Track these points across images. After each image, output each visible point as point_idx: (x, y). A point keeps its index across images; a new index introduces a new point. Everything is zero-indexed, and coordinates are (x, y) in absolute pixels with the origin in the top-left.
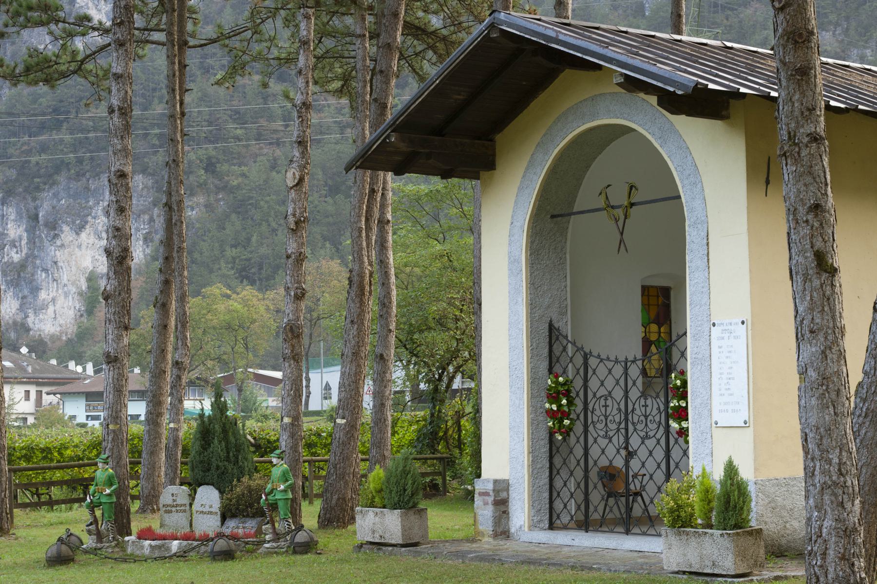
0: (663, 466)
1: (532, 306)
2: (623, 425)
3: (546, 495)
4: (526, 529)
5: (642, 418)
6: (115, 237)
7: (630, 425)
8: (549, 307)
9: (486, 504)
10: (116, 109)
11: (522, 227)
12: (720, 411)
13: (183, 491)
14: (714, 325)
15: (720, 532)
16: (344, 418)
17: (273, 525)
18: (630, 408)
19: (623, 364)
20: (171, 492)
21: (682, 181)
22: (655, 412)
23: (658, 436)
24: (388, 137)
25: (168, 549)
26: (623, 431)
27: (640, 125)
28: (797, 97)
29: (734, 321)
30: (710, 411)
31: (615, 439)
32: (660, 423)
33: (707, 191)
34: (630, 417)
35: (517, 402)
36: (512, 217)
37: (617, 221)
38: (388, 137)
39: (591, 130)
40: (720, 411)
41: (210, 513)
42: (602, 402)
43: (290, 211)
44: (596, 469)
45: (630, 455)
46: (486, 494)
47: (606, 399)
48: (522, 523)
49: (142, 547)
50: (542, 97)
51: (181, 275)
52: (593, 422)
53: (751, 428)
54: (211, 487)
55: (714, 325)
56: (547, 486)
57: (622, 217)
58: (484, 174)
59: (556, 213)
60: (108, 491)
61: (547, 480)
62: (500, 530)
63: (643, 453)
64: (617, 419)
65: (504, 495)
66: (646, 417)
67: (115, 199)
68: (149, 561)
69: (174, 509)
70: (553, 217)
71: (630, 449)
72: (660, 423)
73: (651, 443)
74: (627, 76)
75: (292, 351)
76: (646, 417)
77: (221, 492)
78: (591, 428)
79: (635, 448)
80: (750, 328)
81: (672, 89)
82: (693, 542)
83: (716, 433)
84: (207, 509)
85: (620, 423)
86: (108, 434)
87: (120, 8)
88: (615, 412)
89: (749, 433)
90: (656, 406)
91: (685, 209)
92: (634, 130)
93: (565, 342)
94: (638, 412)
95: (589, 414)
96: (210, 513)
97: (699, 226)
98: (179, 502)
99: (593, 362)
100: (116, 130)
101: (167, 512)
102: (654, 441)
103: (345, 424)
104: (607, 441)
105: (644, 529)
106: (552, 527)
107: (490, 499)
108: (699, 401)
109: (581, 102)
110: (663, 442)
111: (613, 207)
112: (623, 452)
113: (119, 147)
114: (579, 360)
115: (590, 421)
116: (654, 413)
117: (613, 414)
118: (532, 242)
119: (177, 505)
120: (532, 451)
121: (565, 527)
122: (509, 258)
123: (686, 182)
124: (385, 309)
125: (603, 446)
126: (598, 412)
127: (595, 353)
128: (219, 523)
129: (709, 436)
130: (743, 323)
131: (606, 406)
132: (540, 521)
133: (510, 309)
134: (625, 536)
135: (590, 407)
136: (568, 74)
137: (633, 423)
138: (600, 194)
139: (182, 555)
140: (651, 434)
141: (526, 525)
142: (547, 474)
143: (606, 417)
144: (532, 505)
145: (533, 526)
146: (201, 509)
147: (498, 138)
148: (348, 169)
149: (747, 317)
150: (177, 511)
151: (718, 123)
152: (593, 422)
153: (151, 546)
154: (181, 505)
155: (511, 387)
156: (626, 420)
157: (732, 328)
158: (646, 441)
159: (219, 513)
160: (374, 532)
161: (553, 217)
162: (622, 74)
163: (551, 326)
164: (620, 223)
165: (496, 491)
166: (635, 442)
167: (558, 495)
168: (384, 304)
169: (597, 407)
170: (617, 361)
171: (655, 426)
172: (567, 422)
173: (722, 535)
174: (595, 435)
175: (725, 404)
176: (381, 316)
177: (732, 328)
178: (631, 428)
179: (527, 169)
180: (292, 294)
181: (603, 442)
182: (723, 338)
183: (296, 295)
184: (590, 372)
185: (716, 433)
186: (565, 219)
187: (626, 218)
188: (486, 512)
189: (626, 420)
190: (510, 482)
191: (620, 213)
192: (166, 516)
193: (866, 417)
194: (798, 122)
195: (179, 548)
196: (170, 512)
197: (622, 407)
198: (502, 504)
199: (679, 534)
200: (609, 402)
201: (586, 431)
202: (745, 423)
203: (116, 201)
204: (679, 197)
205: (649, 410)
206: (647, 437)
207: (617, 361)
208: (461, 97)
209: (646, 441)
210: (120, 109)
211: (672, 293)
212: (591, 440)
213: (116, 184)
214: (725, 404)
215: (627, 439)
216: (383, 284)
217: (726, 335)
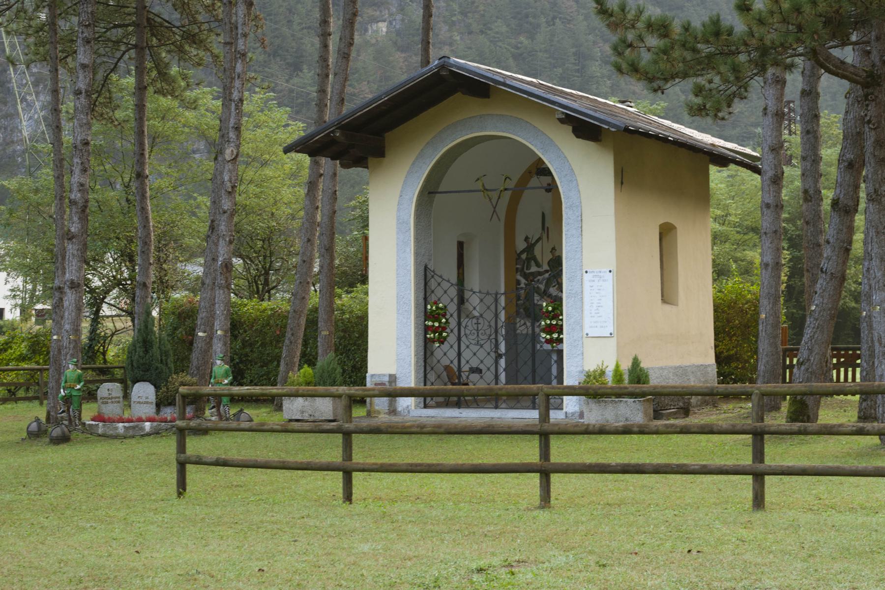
2: (493, 336)
4: (413, 408)
5: (475, 332)
6: (80, 190)
10: (84, 91)
13: (117, 387)
14: (586, 272)
15: (633, 400)
16: (205, 332)
17: (218, 410)
19: (494, 296)
20: (107, 387)
21: (560, 179)
24: (333, 132)
25: (143, 429)
26: (493, 341)
27: (524, 139)
28: (880, 172)
30: (582, 327)
33: (581, 187)
34: (493, 331)
36: (401, 192)
37: (490, 199)
41: (147, 403)
43: (226, 178)
48: (409, 404)
49: (117, 428)
50: (432, 111)
51: (63, 218)
52: (465, 334)
53: (615, 338)
54: (148, 383)
60: (226, 381)
62: (392, 409)
64: (488, 332)
67: (80, 162)
68: (138, 437)
69: (109, 401)
70: (430, 193)
75: (226, 281)
77: (157, 387)
78: (464, 339)
80: (615, 275)
81: (607, 127)
82: (610, 407)
83: (586, 340)
84: (144, 400)
85: (490, 335)
86: (70, 343)
87: (88, 13)
89: (613, 342)
91: (562, 196)
93: (439, 280)
95: (462, 329)
96: (147, 403)
97: (574, 208)
98: (114, 395)
100: (82, 108)
101: (103, 403)
103: (206, 336)
104: (479, 347)
109: (470, 118)
111: (487, 190)
112: (493, 355)
113: (84, 121)
115: (462, 333)
119: (112, 398)
122: (398, 220)
124: (146, 247)
126: (470, 328)
128: (154, 410)
129: (580, 343)
130: (610, 271)
131: (478, 324)
133: (398, 256)
134: (494, 410)
135: (464, 324)
138: (478, 179)
139: (156, 433)
141: (413, 405)
142: (423, 370)
143: (477, 330)
146: (138, 400)
148: (287, 150)
149: (614, 268)
150: (112, 402)
151: (591, 144)
152: (465, 334)
153: (125, 427)
154: (116, 398)
155: (398, 310)
157: (602, 274)
159: (154, 403)
160: (302, 412)
161: (430, 193)
162: (563, 113)
163: (426, 268)
168: (146, 243)
170: (488, 293)
172: (444, 334)
173: (634, 402)
174: (468, 343)
175: (595, 322)
176: (143, 252)
177: (602, 274)
179: (417, 158)
180: (228, 239)
181: (475, 348)
182: (594, 281)
183: (230, 240)
185: (586, 340)
186: (433, 195)
187: (499, 198)
190: (397, 376)
192: (103, 406)
193: (818, 328)
194: (880, 184)
195: (151, 428)
196: (107, 403)
199: (599, 402)
200: (481, 321)
201: (459, 339)
202: (611, 334)
203: (82, 163)
205: (480, 327)
207: (488, 293)
210: (86, 92)
211: (465, 246)
212: (463, 347)
213: (81, 150)
214: (595, 322)
216: (145, 226)
217: (596, 279)
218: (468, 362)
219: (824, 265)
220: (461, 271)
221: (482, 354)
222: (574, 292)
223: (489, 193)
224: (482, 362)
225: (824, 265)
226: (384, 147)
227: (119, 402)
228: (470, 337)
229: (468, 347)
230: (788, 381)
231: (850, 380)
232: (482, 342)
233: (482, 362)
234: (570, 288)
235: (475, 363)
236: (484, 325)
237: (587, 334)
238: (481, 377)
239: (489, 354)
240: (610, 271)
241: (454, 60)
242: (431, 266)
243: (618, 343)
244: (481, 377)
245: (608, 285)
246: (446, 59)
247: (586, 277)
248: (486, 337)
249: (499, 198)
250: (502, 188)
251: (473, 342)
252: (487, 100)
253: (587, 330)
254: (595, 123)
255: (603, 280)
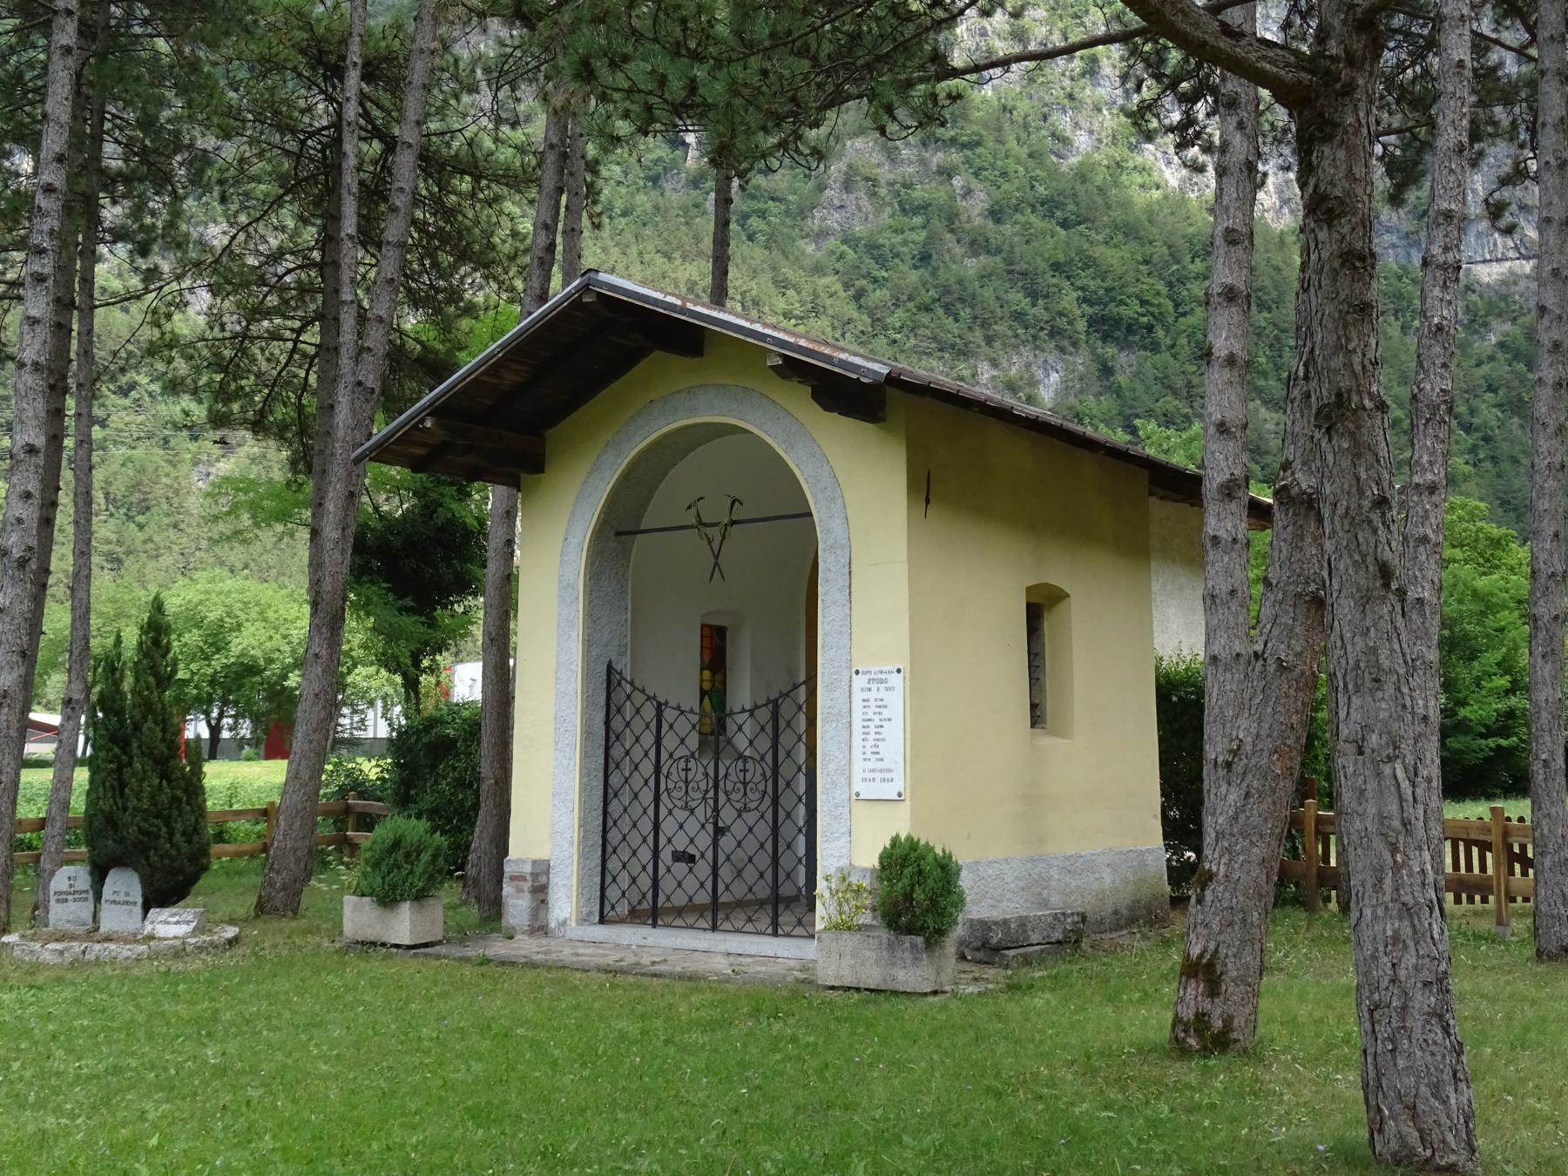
0: (769, 846)
1: (589, 642)
2: (711, 794)
3: (598, 880)
4: (573, 924)
5: (740, 786)
7: (721, 794)
8: (607, 644)
9: (520, 891)
11: (581, 544)
12: (864, 780)
14: (857, 672)
18: (722, 772)
21: (814, 496)
22: (758, 778)
23: (763, 808)
26: (711, 802)
29: (886, 668)
31: (700, 812)
32: (765, 792)
34: (721, 784)
35: (565, 762)
37: (710, 542)
38: (422, 421)
39: (667, 436)
40: (864, 780)
42: (682, 764)
44: (670, 849)
45: (719, 831)
46: (522, 878)
47: (687, 761)
50: (614, 387)
53: (908, 802)
55: (857, 672)
56: (599, 869)
57: (718, 538)
58: (525, 478)
59: (621, 529)
61: (599, 861)
62: (537, 925)
63: (739, 829)
64: (703, 786)
65: (543, 880)
66: (745, 784)
70: (618, 534)
71: (721, 824)
72: (765, 792)
73: (751, 818)
74: (786, 358)
76: (745, 784)
78: (664, 797)
79: (728, 823)
83: (857, 807)
85: (706, 792)
88: (700, 776)
90: (759, 771)
91: (818, 529)
92: (746, 431)
94: (733, 777)
99: (669, 714)
102: (756, 815)
105: (690, 921)
106: (603, 920)
107: (527, 886)
108: (832, 766)
110: (769, 815)
111: (706, 525)
112: (710, 828)
114: (649, 712)
116: (756, 780)
117: (756, 780)
118: (593, 564)
120: (583, 825)
121: (621, 921)
123: (820, 496)
125: (681, 820)
126: (675, 777)
127: (673, 703)
129: (846, 810)
131: (687, 770)
132: (590, 913)
135: (664, 770)
136: (658, 359)
137: (726, 793)
138: (690, 507)
140: (752, 805)
143: (687, 782)
144: (580, 894)
145: (584, 920)
147: (549, 433)
149: (905, 665)
155: (557, 743)
156: (716, 787)
158: (744, 815)
161: (618, 534)
163: (610, 668)
164: (716, 545)
165: (535, 875)
166: (727, 815)
167: (614, 880)
169: (673, 770)
171: (757, 796)
175: (873, 771)
178: (722, 798)
179: (591, 473)
181: (681, 815)
184: (665, 727)
187: (724, 538)
188: (520, 902)
189: (716, 787)
191: (715, 533)
197: (711, 772)
198: (540, 892)
202: (900, 795)
204: (810, 514)
205: (749, 776)
206: (746, 809)
208: (517, 379)
209: (744, 815)
212: (663, 812)
214: (873, 771)
215: (716, 810)
217: (874, 686)
218: (669, 840)
219: (1426, 707)
220: (81, 594)
221: (692, 826)
222: (835, 711)
223: (709, 531)
224: (692, 841)
225: (1426, 707)
226: (543, 454)
227: (86, 899)
228: (675, 794)
229: (670, 812)
230: (1461, 844)
231: (1476, 870)
232: (693, 804)
233: (692, 841)
234: (829, 703)
235: (681, 843)
236: (755, 773)
237: (858, 794)
238: (691, 870)
239: (703, 826)
240: (899, 671)
241: (603, 277)
242: (624, 665)
243: (913, 813)
244: (691, 870)
245: (895, 699)
246: (591, 275)
247: (859, 682)
248: (699, 795)
249: (724, 538)
250: (726, 520)
251: (679, 804)
252: (698, 359)
253: (858, 786)
254: (836, 370)
255: (887, 689)
